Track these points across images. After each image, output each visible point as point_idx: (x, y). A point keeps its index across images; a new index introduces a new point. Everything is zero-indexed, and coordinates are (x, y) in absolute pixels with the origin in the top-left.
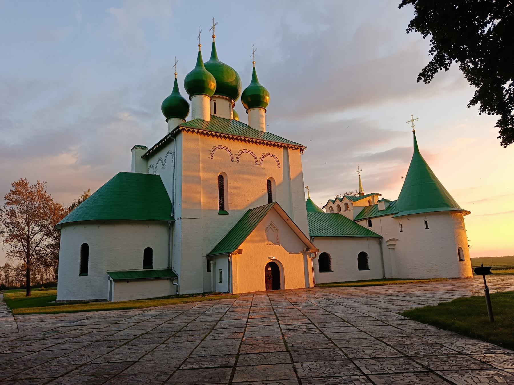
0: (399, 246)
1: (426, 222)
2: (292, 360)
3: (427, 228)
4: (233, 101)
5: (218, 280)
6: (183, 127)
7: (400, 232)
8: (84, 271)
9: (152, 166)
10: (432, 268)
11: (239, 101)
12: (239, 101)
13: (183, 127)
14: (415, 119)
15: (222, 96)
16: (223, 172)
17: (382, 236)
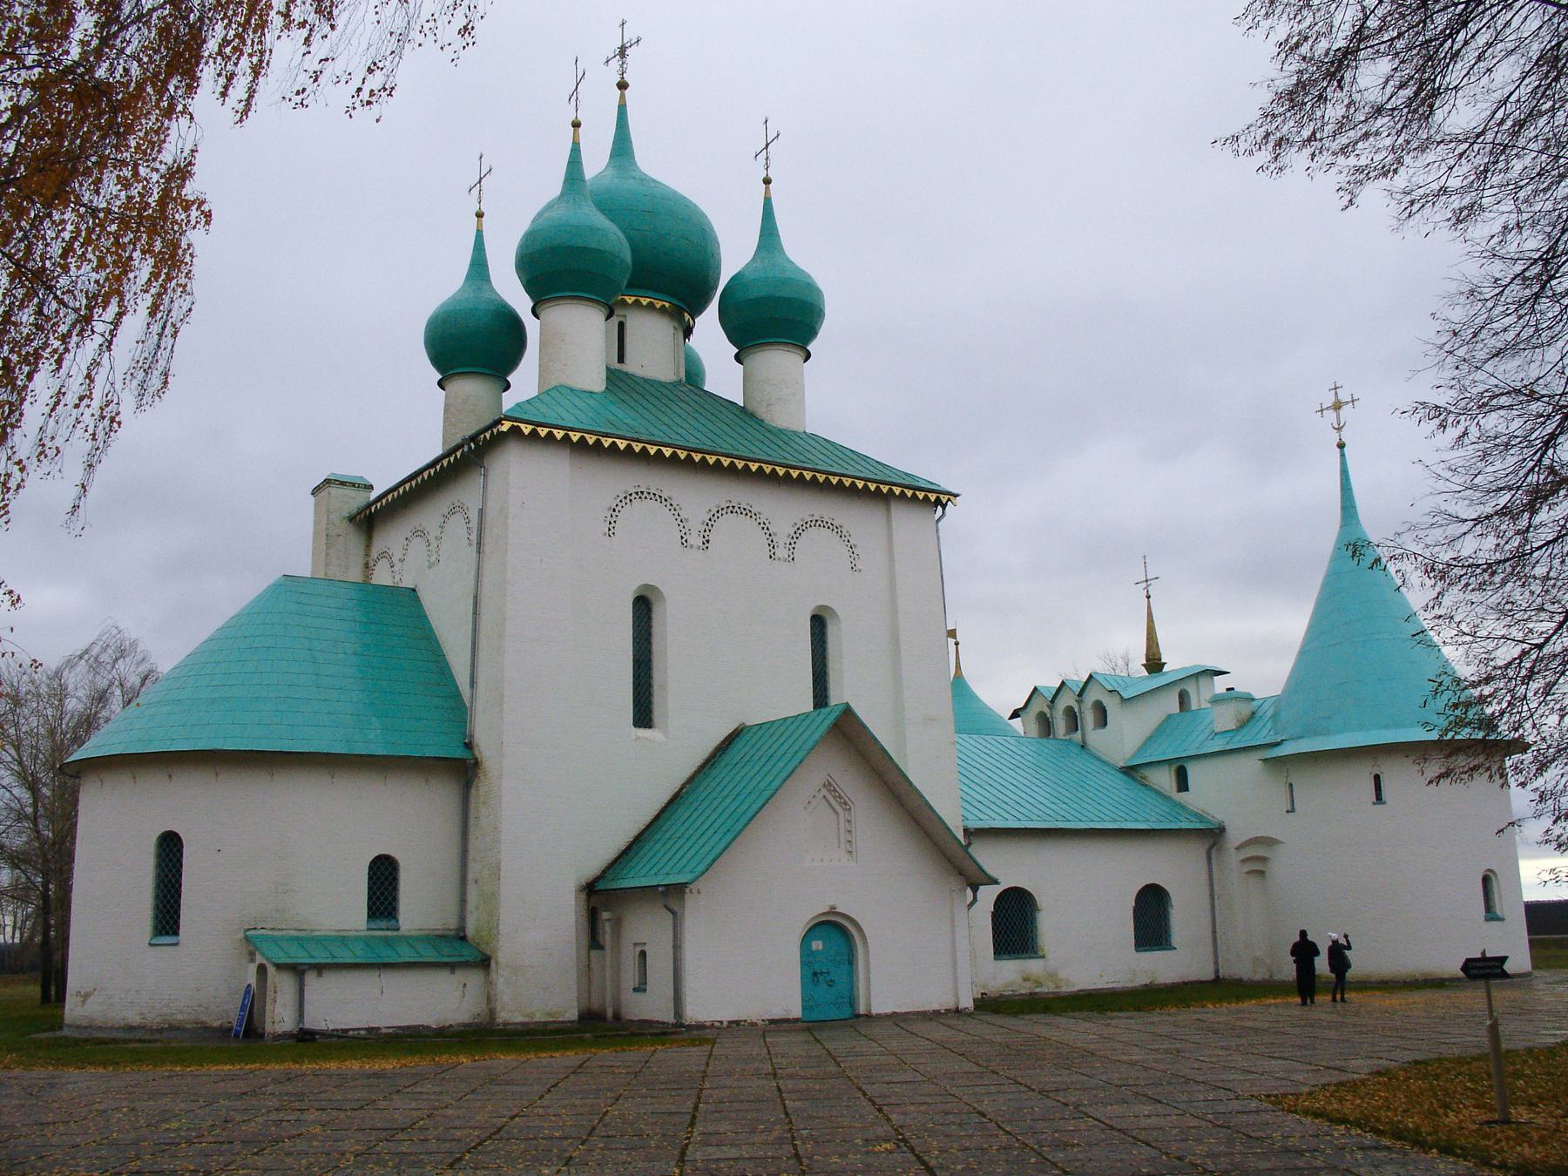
0: (1281, 865)
1: (1377, 778)
4: (687, 316)
5: (630, 976)
6: (515, 424)
7: (1287, 812)
8: (167, 919)
9: (384, 555)
11: (708, 323)
12: (708, 323)
13: (515, 424)
15: (649, 300)
16: (826, 608)
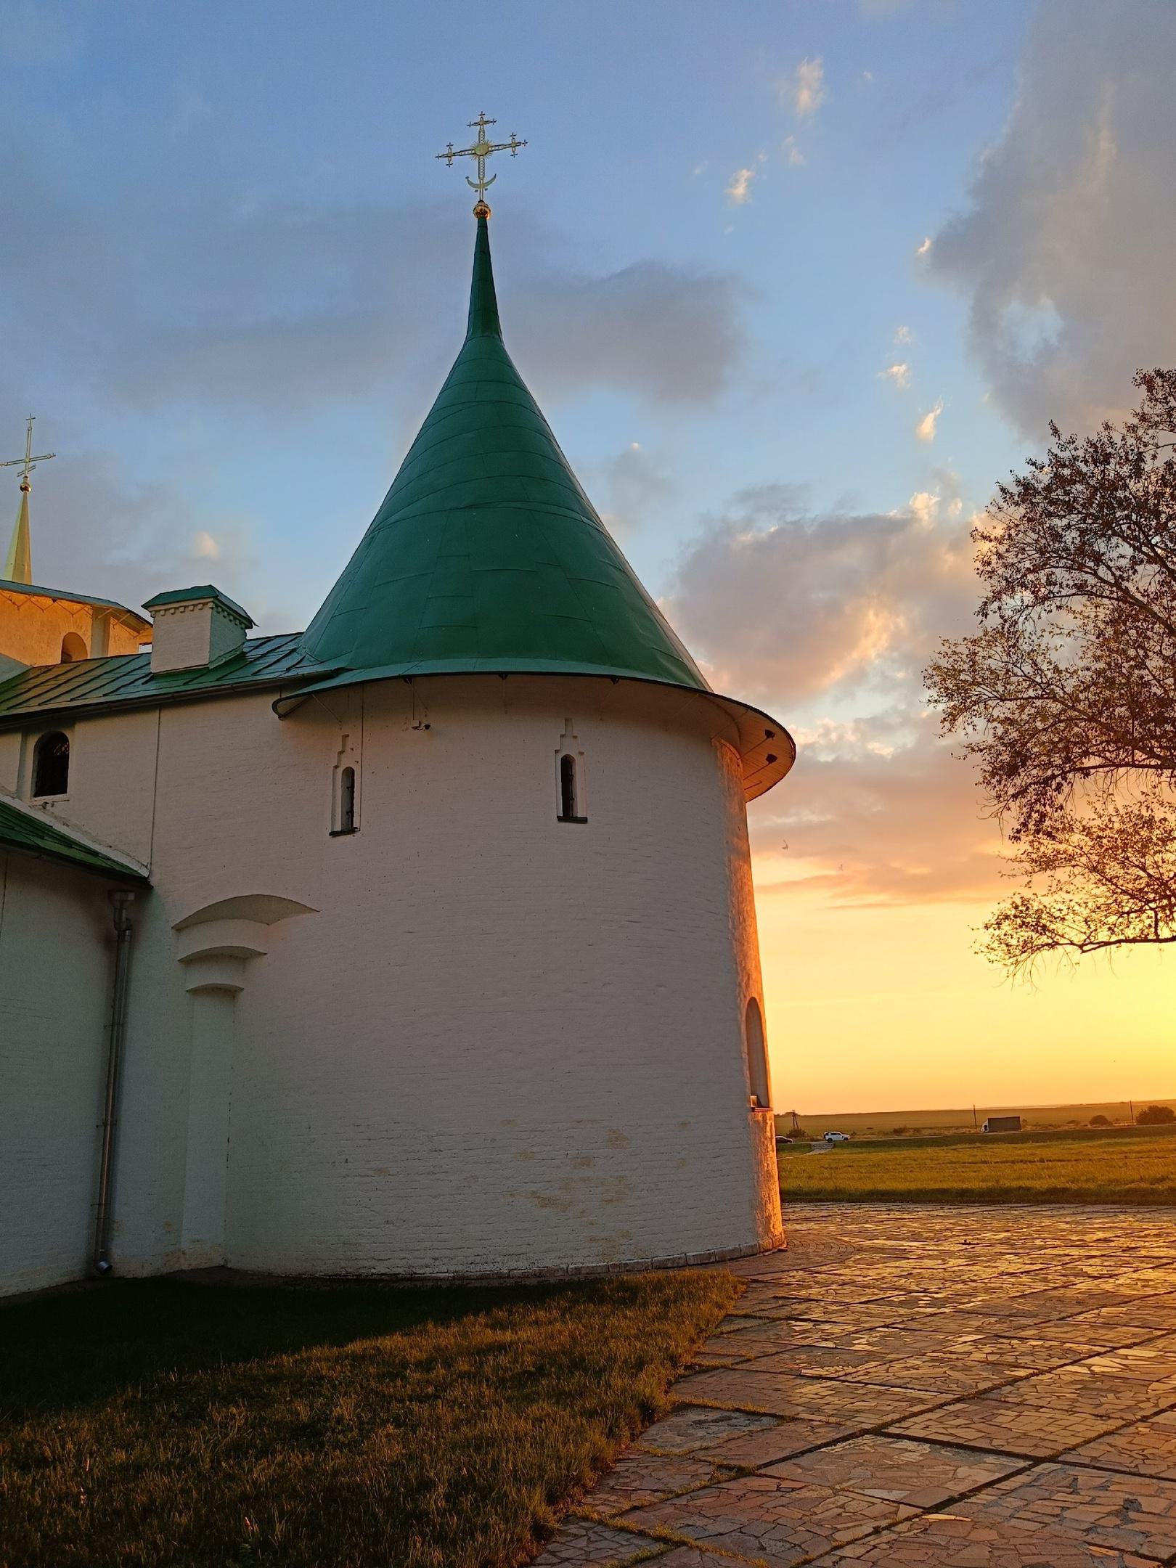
1: (567, 764)
2: (510, 146)
3: (568, 815)
7: (334, 834)
10: (586, 1161)
14: (500, 147)
17: (144, 873)
